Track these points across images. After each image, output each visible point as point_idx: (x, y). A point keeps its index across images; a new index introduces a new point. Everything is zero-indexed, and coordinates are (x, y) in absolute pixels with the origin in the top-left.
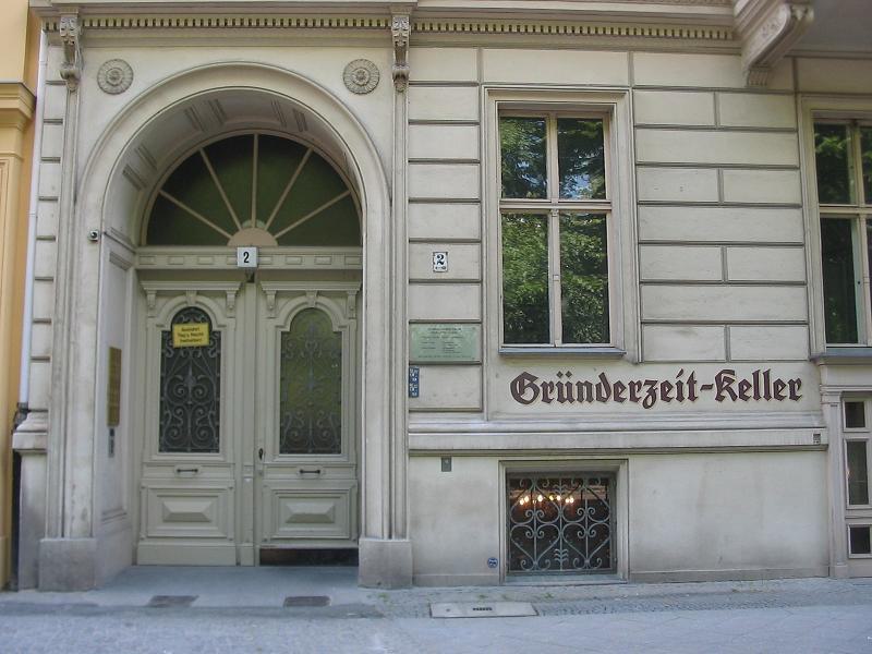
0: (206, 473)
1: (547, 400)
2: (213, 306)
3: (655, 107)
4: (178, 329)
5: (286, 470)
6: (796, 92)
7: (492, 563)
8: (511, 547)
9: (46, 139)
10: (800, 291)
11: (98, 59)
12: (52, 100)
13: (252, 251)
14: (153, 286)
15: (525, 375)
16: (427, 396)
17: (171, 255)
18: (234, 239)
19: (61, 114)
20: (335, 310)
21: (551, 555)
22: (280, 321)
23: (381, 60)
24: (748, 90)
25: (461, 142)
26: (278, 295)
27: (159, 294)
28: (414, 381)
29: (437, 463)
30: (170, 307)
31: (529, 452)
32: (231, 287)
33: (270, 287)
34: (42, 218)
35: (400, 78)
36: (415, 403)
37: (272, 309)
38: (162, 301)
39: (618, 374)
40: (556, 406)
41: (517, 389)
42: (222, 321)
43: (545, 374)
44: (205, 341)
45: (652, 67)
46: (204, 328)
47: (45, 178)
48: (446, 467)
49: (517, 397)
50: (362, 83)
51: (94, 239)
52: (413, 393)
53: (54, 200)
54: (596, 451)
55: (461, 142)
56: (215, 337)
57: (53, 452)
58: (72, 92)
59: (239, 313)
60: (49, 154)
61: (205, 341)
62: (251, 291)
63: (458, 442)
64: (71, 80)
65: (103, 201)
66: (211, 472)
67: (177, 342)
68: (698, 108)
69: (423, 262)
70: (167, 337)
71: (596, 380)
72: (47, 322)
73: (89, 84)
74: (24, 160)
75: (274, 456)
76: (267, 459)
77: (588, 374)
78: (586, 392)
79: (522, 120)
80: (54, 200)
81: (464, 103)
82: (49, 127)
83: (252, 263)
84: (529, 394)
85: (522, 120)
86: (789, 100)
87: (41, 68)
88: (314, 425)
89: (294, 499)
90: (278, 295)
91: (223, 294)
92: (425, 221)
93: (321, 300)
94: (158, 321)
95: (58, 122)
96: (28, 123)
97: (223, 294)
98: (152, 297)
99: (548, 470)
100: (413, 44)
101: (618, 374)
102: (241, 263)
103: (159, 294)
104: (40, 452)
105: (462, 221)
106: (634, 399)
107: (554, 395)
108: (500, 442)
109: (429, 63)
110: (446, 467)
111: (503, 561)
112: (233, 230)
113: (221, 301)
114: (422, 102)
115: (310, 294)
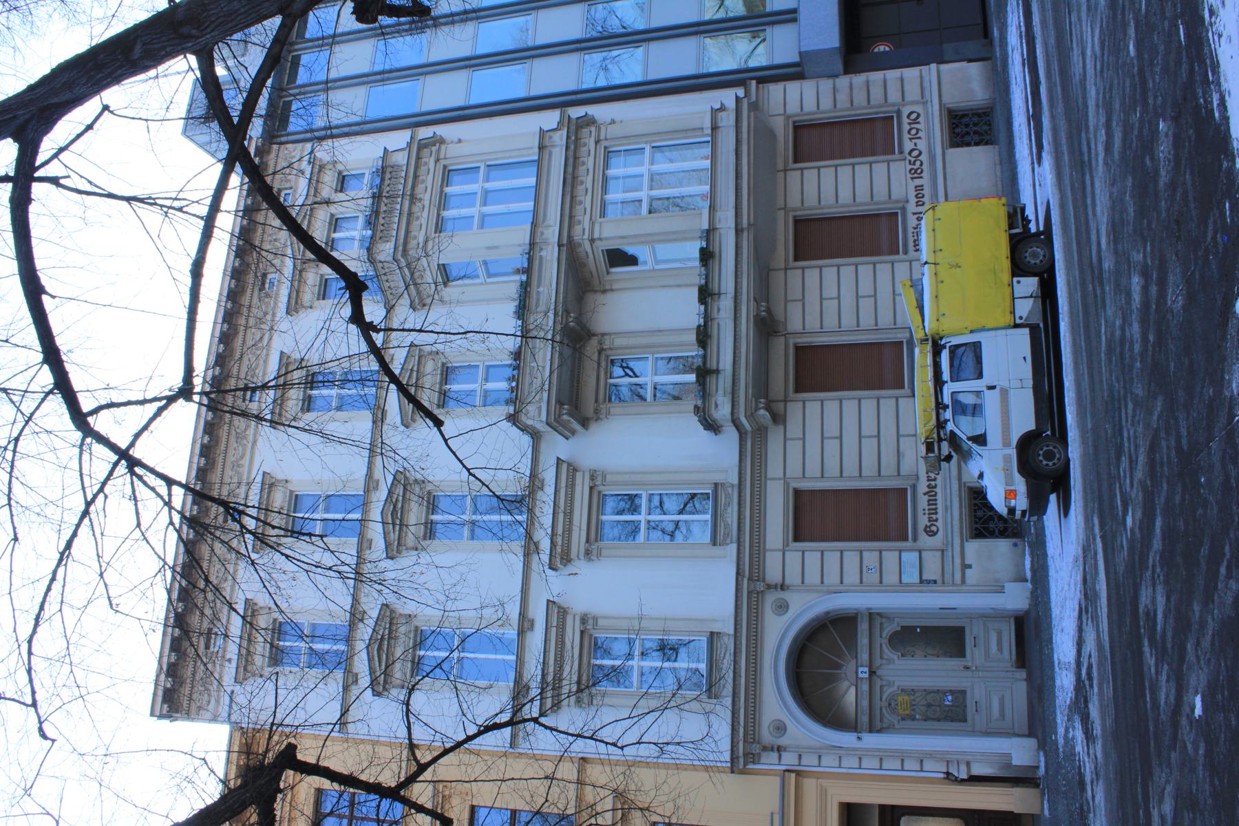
1: (936, 520)
2: (888, 692)
3: (794, 468)
5: (974, 654)
6: (785, 401)
7: (1015, 545)
8: (1007, 537)
9: (809, 761)
10: (882, 401)
11: (767, 736)
12: (789, 759)
13: (860, 669)
15: (925, 530)
16: (937, 577)
20: (889, 629)
21: (980, 509)
22: (895, 657)
23: (770, 599)
24: (784, 423)
25: (813, 559)
26: (881, 658)
27: (881, 721)
28: (929, 582)
29: (968, 571)
31: (961, 528)
32: (878, 683)
33: (878, 662)
35: (783, 587)
36: (940, 581)
37: (890, 661)
39: (923, 487)
40: (940, 516)
41: (931, 533)
42: (895, 688)
43: (923, 521)
45: (774, 468)
48: (970, 566)
49: (935, 534)
50: (782, 607)
51: (859, 738)
52: (935, 582)
54: (960, 497)
55: (813, 559)
58: (785, 750)
59: (891, 679)
62: (879, 672)
63: (958, 561)
64: (779, 749)
66: (976, 693)
68: (794, 448)
69: (872, 577)
71: (927, 497)
73: (783, 741)
74: (818, 776)
75: (968, 660)
76: (969, 664)
77: (923, 501)
78: (932, 502)
79: (801, 531)
81: (793, 558)
82: (804, 762)
83: (866, 669)
84: (934, 528)
85: (801, 531)
86: (789, 404)
88: (947, 638)
89: (992, 648)
90: (881, 658)
92: (852, 576)
93: (884, 635)
95: (800, 756)
97: (881, 687)
99: (941, 723)
100: (764, 581)
101: (923, 487)
102: (867, 676)
103: (881, 721)
104: (968, 764)
105: (851, 559)
106: (935, 479)
107: (934, 517)
108: (957, 541)
109: (773, 573)
110: (970, 566)
111: (1015, 540)
114: (793, 578)
115: (882, 641)
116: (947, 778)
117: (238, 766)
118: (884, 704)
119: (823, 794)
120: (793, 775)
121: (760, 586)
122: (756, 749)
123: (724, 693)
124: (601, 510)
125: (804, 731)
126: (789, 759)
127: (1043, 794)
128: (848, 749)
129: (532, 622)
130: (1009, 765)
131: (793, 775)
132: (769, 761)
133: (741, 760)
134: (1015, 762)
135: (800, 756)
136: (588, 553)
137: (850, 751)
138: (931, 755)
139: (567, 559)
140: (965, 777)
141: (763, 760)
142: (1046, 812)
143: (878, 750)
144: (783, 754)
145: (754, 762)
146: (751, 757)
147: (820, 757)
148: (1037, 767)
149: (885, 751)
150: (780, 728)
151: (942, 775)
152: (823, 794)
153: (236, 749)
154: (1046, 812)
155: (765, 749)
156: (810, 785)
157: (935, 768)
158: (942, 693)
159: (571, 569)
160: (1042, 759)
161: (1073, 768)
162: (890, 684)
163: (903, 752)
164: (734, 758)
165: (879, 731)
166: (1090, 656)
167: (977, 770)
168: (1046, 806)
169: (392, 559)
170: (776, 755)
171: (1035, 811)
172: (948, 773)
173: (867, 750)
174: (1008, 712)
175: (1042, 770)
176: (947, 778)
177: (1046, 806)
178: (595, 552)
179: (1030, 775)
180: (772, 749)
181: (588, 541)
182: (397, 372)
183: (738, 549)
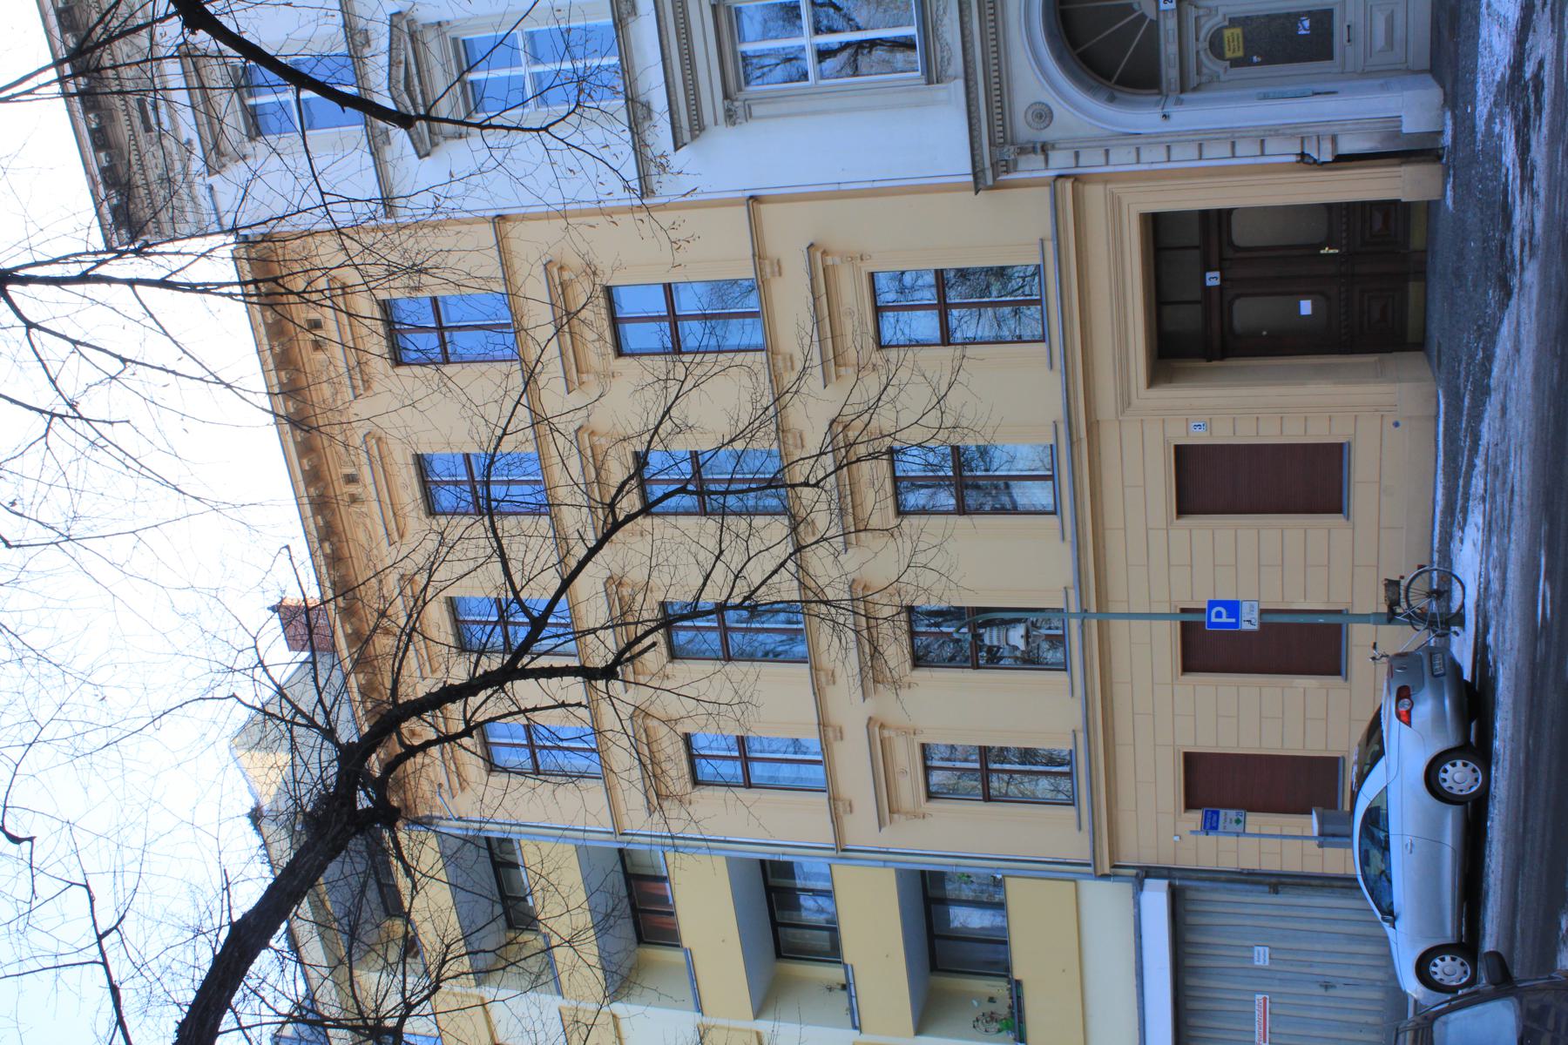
0: (1350, 18)
2: (1208, 26)
4: (1229, 54)
9: (1092, 162)
11: (1024, 130)
12: (1061, 161)
13: (1209, 275)
14: (1194, 79)
17: (1167, 32)
18: (1151, 15)
19: (1071, 153)
27: (1199, 73)
30: (1211, 65)
34: (1154, 157)
38: (1205, 71)
42: (1220, 17)
44: (1238, 31)
46: (1227, 33)
47: (1122, 159)
51: (1165, 116)
53: (1138, 150)
56: (1234, 22)
57: (1335, 129)
58: (1053, 147)
60: (1102, 160)
61: (1238, 31)
64: (1045, 149)
65: (1142, 117)
67: (1240, 54)
70: (1236, 63)
72: (1233, 144)
73: (1048, 135)
74: (1106, 179)
80: (1138, 150)
82: (1082, 161)
87: (1035, 174)
91: (1197, 18)
94: (1221, 71)
95: (1077, 155)
96: (1076, 179)
97: (1197, 18)
98: (1204, 79)
103: (1199, 73)
104: (1334, 140)
112: (1143, 17)
113: (1203, 20)
116: (1302, 160)
117: (274, 356)
118: (1204, 45)
119: (1115, 205)
120: (1069, 185)
121: (1009, 152)
122: (1009, 152)
123: (951, 71)
124: (738, 35)
125: (1079, 113)
126: (1061, 161)
127: (1446, 176)
128: (1149, 135)
129: (647, 107)
130: (1397, 134)
131: (1069, 185)
132: (1031, 168)
133: (989, 174)
134: (1406, 129)
135: (1077, 155)
136: (730, 116)
137: (1154, 138)
138: (1276, 132)
139: (698, 128)
140: (1330, 159)
141: (1021, 166)
142: (1449, 202)
143: (1196, 132)
144: (1052, 154)
145: (1007, 172)
146: (1003, 166)
147: (1107, 151)
148: (1441, 133)
149: (1206, 131)
150: (1043, 115)
151: (1293, 159)
152: (1115, 205)
153: (271, 366)
154: (1449, 202)
155: (1023, 151)
156: (1095, 195)
157: (1283, 151)
158: (1293, 18)
159: (705, 140)
160: (1449, 123)
161: (1497, 179)
162: (1211, 11)
163: (1232, 130)
164: (977, 173)
165: (1195, 89)
166: (1541, 64)
167: (1346, 147)
168: (1449, 193)
169: (428, 154)
170: (1041, 157)
171: (1432, 195)
172: (1303, 155)
173: (1178, 133)
174: (1399, 33)
175: (1447, 139)
176: (1302, 160)
177: (1449, 193)
178: (740, 112)
179: (1429, 146)
180: (1034, 150)
181: (726, 96)
182: (390, 105)
183: (967, 87)
